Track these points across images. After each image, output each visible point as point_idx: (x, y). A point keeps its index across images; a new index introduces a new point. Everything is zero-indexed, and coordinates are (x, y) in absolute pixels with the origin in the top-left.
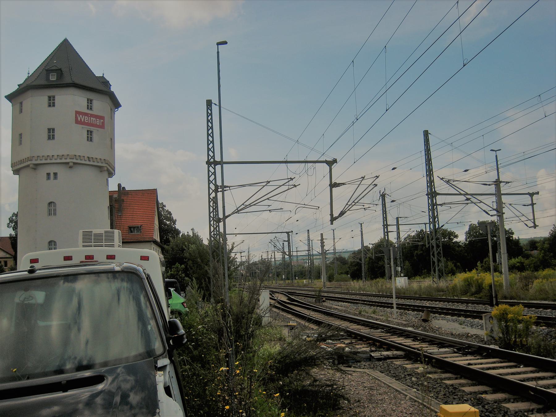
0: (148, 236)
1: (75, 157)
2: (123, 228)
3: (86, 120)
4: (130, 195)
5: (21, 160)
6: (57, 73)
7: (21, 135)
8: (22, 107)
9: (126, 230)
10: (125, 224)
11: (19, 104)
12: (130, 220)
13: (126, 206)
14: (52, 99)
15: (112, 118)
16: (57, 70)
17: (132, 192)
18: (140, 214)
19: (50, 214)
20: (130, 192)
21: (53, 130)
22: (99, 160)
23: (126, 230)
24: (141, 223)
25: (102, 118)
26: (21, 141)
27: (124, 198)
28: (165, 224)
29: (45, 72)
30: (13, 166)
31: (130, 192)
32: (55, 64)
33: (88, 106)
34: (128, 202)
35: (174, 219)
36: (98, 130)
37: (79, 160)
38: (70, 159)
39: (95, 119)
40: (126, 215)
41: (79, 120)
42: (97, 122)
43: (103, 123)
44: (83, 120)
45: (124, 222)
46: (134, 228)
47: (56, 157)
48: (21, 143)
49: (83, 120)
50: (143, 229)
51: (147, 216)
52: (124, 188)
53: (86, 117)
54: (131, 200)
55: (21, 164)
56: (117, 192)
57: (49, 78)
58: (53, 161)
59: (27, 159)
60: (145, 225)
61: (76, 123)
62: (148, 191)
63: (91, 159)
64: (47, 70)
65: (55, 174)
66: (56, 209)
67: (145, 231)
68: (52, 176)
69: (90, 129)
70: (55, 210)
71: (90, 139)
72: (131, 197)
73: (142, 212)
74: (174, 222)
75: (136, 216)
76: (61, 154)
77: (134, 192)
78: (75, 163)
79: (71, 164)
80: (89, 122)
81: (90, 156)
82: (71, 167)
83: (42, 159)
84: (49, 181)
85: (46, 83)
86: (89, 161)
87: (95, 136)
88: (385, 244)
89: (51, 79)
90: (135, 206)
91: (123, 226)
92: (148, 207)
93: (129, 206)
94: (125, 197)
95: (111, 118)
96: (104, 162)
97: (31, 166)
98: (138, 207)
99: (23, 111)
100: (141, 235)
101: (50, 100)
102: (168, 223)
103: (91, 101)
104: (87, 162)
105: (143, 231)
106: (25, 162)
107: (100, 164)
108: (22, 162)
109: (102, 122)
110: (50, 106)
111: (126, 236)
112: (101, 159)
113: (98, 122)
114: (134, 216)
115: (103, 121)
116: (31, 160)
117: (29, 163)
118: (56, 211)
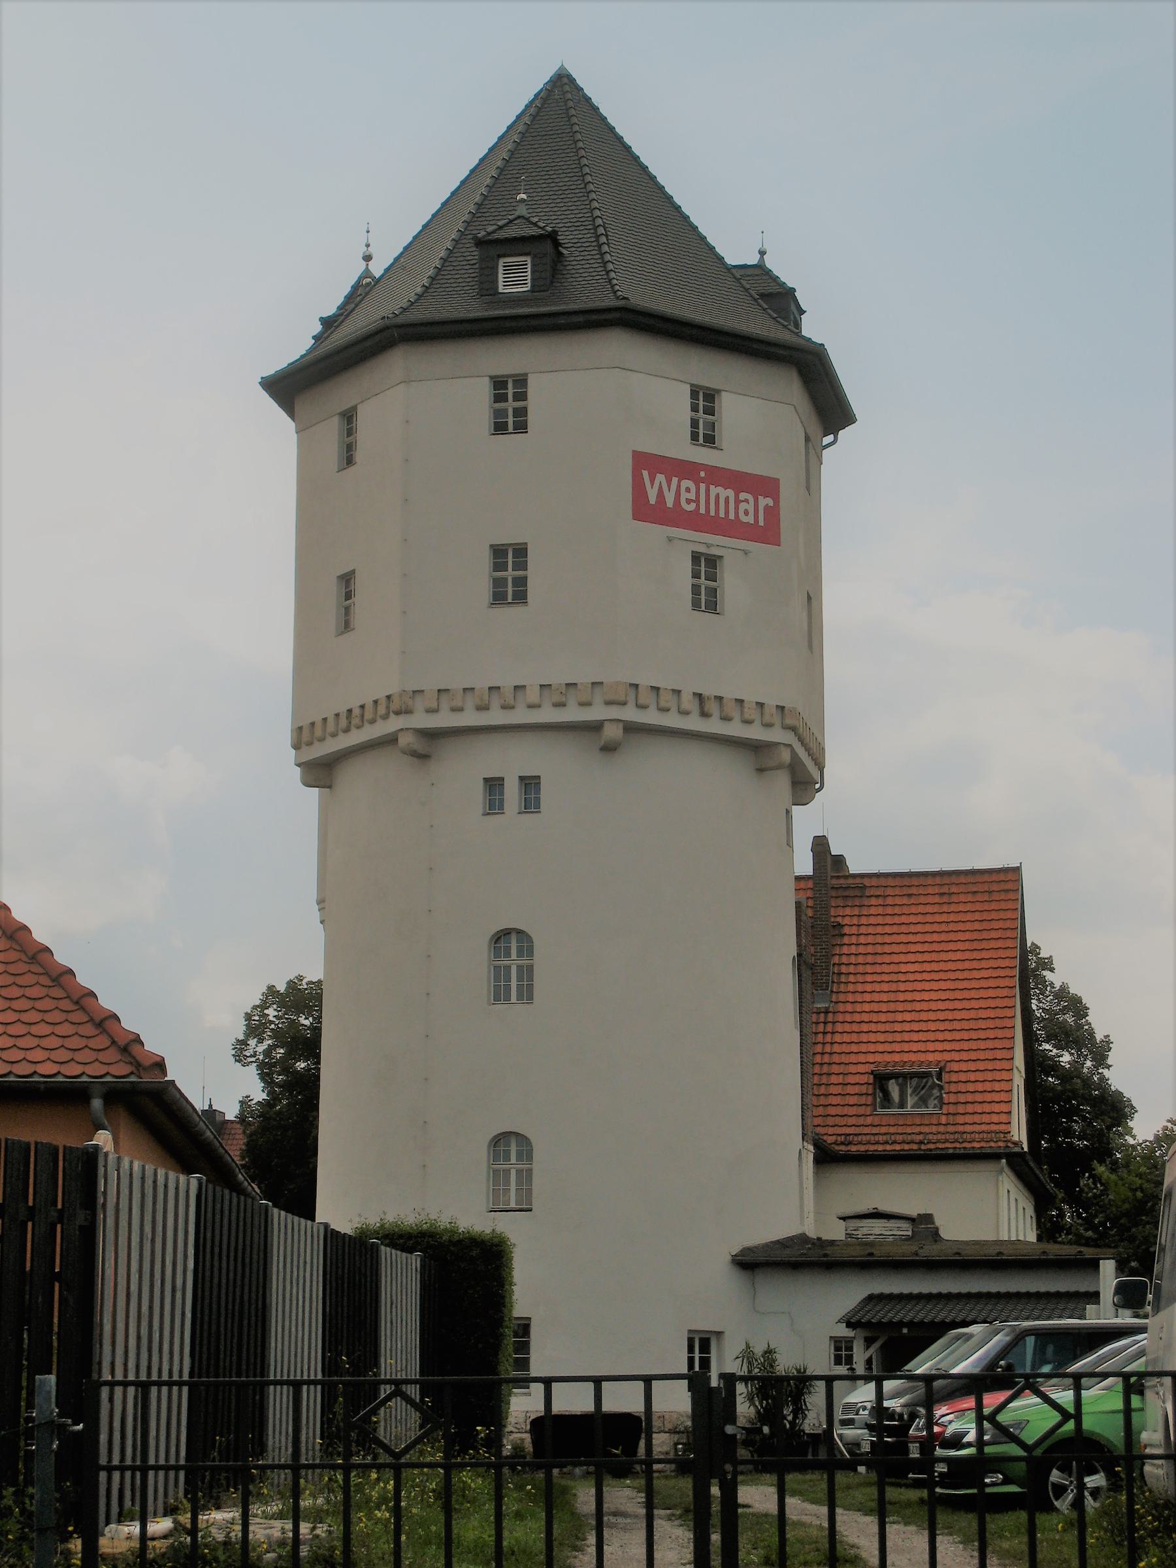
0: (977, 1128)
1: (653, 695)
2: (840, 1079)
3: (689, 501)
4: (873, 901)
5: (350, 711)
6: (534, 257)
7: (347, 580)
8: (350, 432)
9: (856, 1089)
10: (853, 1059)
11: (336, 420)
12: (881, 1037)
13: (853, 959)
14: (510, 391)
15: (811, 483)
16: (532, 239)
17: (882, 882)
18: (933, 1006)
19: (500, 994)
20: (874, 882)
21: (521, 551)
22: (751, 713)
23: (856, 1089)
24: (938, 1057)
25: (766, 486)
26: (347, 610)
27: (844, 914)
28: (1053, 1067)
29: (475, 254)
30: (302, 737)
31: (874, 882)
32: (522, 210)
33: (694, 423)
34: (862, 940)
35: (1099, 1037)
36: (746, 553)
37: (652, 710)
38: (608, 703)
39: (730, 493)
40: (858, 1008)
41: (652, 500)
42: (743, 506)
43: (773, 514)
44: (670, 503)
45: (845, 1048)
46: (903, 1078)
47: (533, 695)
48: (346, 625)
49: (670, 503)
50: (953, 1088)
51: (972, 1014)
52: (839, 861)
53: (686, 483)
54: (879, 929)
55: (347, 730)
56: (810, 884)
57: (496, 281)
58: (521, 716)
59: (383, 703)
60: (964, 1067)
62: (970, 879)
63: (712, 707)
64: (480, 243)
65: (530, 784)
66: (530, 968)
67: (962, 1098)
68: (512, 792)
69: (708, 546)
70: (527, 973)
72: (880, 910)
73: (943, 995)
74: (1100, 1054)
75: (908, 1016)
76: (558, 678)
77: (898, 882)
78: (631, 729)
79: (612, 732)
80: (702, 511)
81: (706, 692)
82: (609, 748)
83: (460, 704)
84: (495, 820)
85: (476, 310)
86: (704, 714)
87: (731, 583)
88: (579, 1543)
91: (842, 1069)
92: (975, 964)
93: (870, 959)
94: (848, 911)
95: (808, 488)
96: (777, 720)
97: (405, 740)
98: (916, 967)
99: (359, 456)
100: (943, 1120)
101: (500, 398)
102: (1066, 1058)
103: (711, 396)
104: (694, 723)
105: (952, 1098)
106: (373, 721)
107: (755, 733)
108: (356, 721)
109: (767, 508)
110: (500, 428)
111: (861, 1121)
112: (761, 705)
113: (749, 509)
114: (899, 1017)
116: (407, 711)
117: (393, 724)
118: (531, 978)
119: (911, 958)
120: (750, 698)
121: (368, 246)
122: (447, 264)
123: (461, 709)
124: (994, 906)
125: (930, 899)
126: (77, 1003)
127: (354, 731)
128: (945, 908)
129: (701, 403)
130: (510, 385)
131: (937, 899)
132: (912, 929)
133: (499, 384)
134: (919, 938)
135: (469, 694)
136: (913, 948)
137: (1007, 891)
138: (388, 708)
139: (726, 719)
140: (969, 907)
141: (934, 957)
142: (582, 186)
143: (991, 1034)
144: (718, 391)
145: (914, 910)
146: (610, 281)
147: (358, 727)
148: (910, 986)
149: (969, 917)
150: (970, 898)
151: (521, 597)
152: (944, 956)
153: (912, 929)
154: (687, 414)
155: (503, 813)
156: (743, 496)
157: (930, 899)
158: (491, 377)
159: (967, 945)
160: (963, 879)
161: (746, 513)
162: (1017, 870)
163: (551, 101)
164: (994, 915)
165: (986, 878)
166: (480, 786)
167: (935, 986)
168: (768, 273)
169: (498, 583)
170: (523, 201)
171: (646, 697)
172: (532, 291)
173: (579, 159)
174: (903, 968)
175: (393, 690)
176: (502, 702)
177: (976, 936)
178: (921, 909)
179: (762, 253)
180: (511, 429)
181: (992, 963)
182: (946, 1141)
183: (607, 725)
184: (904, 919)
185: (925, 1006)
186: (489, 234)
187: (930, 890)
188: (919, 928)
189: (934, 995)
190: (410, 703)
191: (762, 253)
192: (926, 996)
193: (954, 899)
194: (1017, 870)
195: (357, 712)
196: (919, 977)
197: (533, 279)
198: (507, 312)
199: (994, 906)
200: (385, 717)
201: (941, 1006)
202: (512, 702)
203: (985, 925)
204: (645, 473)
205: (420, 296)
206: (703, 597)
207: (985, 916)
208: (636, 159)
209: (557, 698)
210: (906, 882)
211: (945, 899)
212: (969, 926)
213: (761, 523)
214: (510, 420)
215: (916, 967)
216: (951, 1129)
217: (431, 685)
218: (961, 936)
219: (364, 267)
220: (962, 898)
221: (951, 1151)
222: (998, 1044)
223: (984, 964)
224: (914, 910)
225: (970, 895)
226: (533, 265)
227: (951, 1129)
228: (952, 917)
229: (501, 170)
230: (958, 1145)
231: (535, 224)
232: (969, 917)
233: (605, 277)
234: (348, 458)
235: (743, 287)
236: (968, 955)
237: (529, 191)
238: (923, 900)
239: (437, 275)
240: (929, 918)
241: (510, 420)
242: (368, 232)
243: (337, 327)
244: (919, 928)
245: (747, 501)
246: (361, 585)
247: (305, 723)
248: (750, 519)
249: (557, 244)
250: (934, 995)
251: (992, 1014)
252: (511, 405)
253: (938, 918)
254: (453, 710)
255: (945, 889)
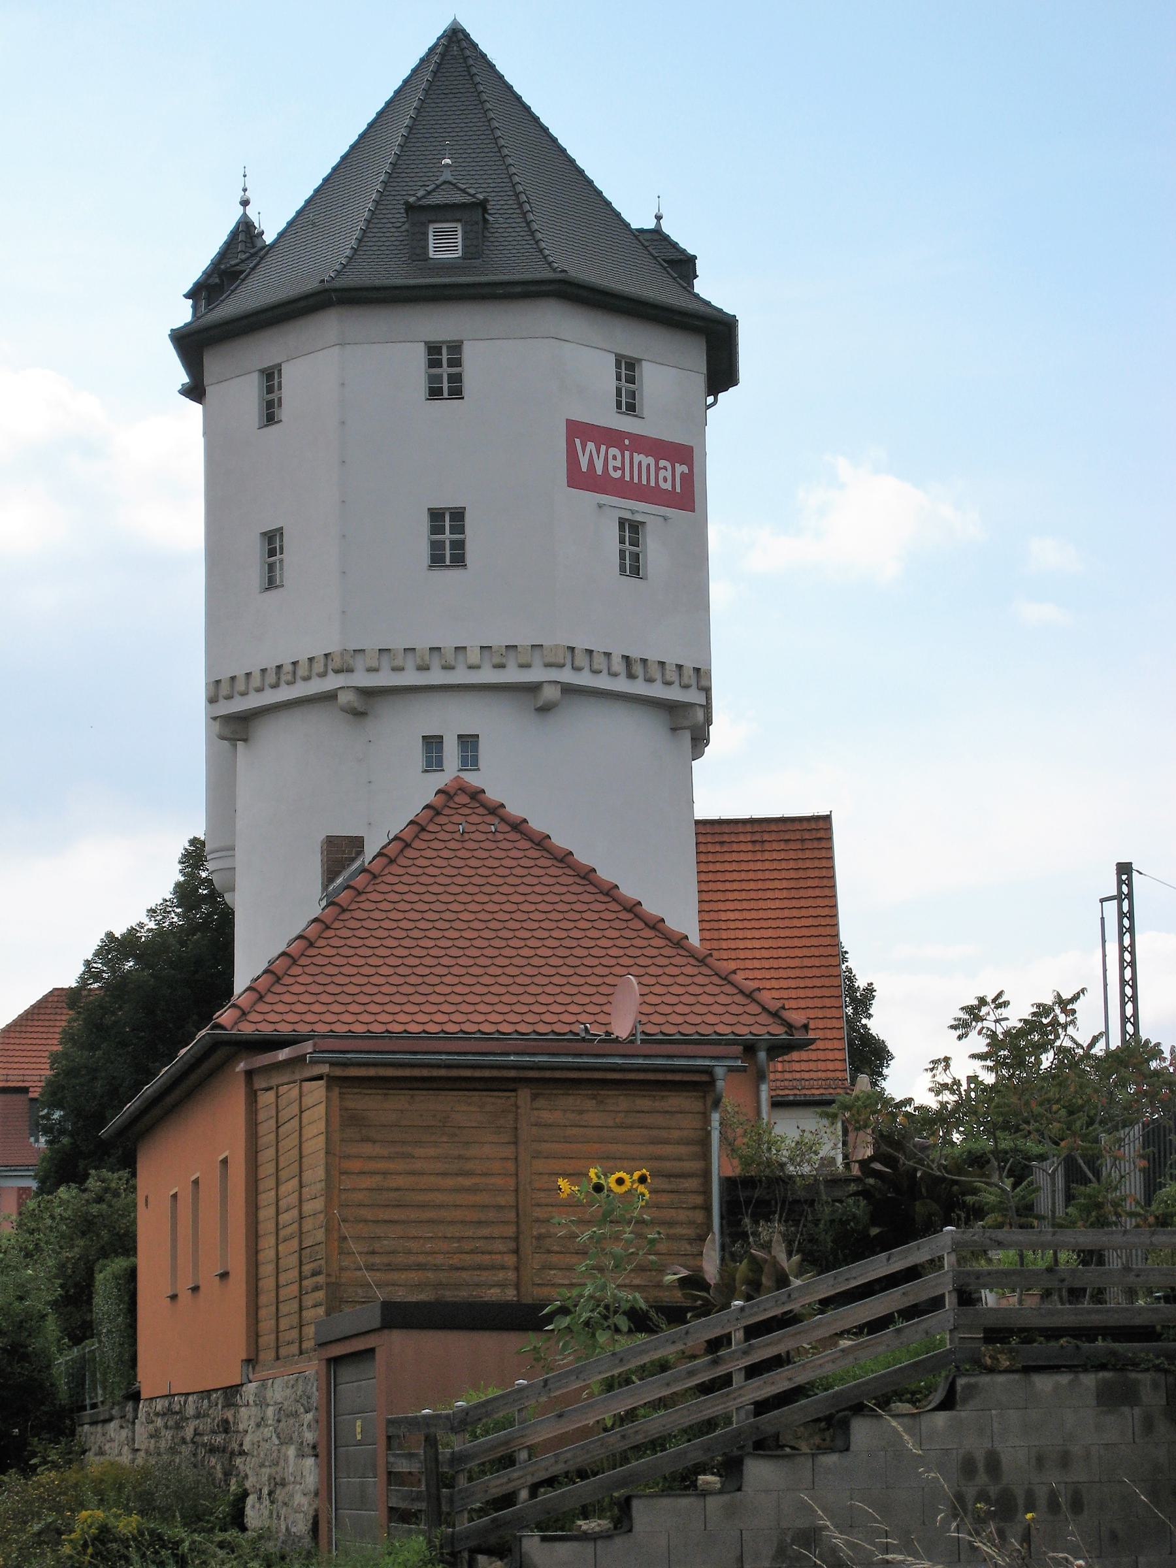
3: (615, 469)
11: (255, 377)
14: (445, 357)
16: (464, 206)
18: (757, 954)
21: (458, 515)
26: (271, 567)
30: (216, 692)
32: (447, 176)
35: (861, 983)
36: (665, 519)
37: (658, 684)
38: (548, 665)
39: (651, 460)
41: (584, 469)
42: (662, 473)
44: (599, 472)
47: (474, 657)
49: (599, 472)
53: (613, 451)
57: (426, 247)
61: (572, 483)
62: (782, 827)
63: (638, 669)
64: (410, 208)
65: (469, 743)
69: (633, 512)
71: (632, 566)
76: (499, 640)
78: (569, 690)
80: (627, 478)
81: (635, 654)
82: (545, 709)
85: (398, 275)
86: (631, 676)
87: (654, 550)
89: (431, 254)
90: (721, 906)
92: (795, 913)
97: (344, 698)
98: (737, 915)
99: (285, 413)
101: (434, 363)
104: (622, 685)
106: (307, 679)
108: (284, 678)
109: (682, 474)
110: (435, 393)
113: (590, 455)
115: (685, 469)
117: (332, 682)
119: (730, 905)
120: (671, 660)
121: (245, 190)
122: (371, 226)
123: (401, 669)
124: (808, 854)
125: (743, 847)
126: (725, 979)
127: (284, 687)
128: (759, 856)
129: (623, 372)
130: (444, 351)
131: (750, 847)
132: (728, 876)
133: (433, 350)
134: (735, 886)
135: (410, 655)
136: (731, 896)
137: (819, 839)
138: (326, 665)
139: (650, 680)
140: (782, 855)
141: (752, 905)
142: (496, 149)
143: (818, 982)
144: (640, 361)
145: (727, 857)
146: (541, 251)
147: (288, 683)
148: (732, 934)
149: (784, 865)
150: (782, 846)
151: (459, 560)
152: (762, 904)
153: (728, 876)
154: (613, 383)
155: (443, 770)
156: (662, 463)
157: (743, 847)
158: (426, 343)
159: (785, 894)
160: (774, 827)
161: (665, 480)
162: (827, 819)
163: (449, 57)
164: (808, 864)
165: (798, 826)
166: (419, 744)
167: (757, 934)
168: (666, 238)
169: (436, 546)
170: (448, 165)
171: (582, 660)
172: (463, 258)
173: (489, 121)
174: (723, 916)
175: (333, 647)
176: (443, 662)
177: (792, 884)
178: (735, 857)
179: (659, 218)
180: (446, 395)
181: (812, 912)
182: (786, 1088)
183: (545, 685)
184: (718, 867)
185: (749, 954)
186: (419, 199)
187: (742, 838)
188: (735, 876)
189: (757, 944)
190: (351, 662)
191: (659, 218)
192: (749, 944)
193: (767, 846)
194: (827, 819)
195: (288, 668)
196: (740, 925)
197: (465, 247)
198: (447, 280)
199: (808, 854)
200: (323, 675)
201: (765, 953)
202: (453, 663)
203: (801, 874)
204: (578, 441)
205: (350, 259)
206: (628, 562)
207: (800, 864)
208: (536, 119)
209: (497, 660)
210: (717, 829)
211: (758, 847)
212: (784, 874)
213: (678, 490)
214: (445, 386)
215: (737, 915)
216: (788, 1076)
217: (371, 643)
218: (777, 884)
219: (242, 212)
220: (775, 846)
221: (791, 1098)
222: (826, 992)
223: (804, 912)
224: (727, 857)
225: (782, 843)
226: (465, 232)
227: (788, 1076)
228: (767, 865)
229: (410, 128)
230: (797, 1092)
231: (463, 191)
232: (784, 865)
233: (535, 246)
234: (270, 416)
235: (651, 254)
236: (787, 904)
237: (454, 156)
238: (735, 847)
239: (363, 237)
240: (744, 866)
241: (445, 386)
242: (245, 176)
243: (243, 280)
244: (735, 876)
245: (665, 468)
246: (290, 542)
247: (225, 675)
248: (668, 486)
249: (485, 210)
250: (757, 944)
251: (817, 962)
252: (445, 371)
253: (752, 866)
254: (394, 669)
255: (757, 837)
